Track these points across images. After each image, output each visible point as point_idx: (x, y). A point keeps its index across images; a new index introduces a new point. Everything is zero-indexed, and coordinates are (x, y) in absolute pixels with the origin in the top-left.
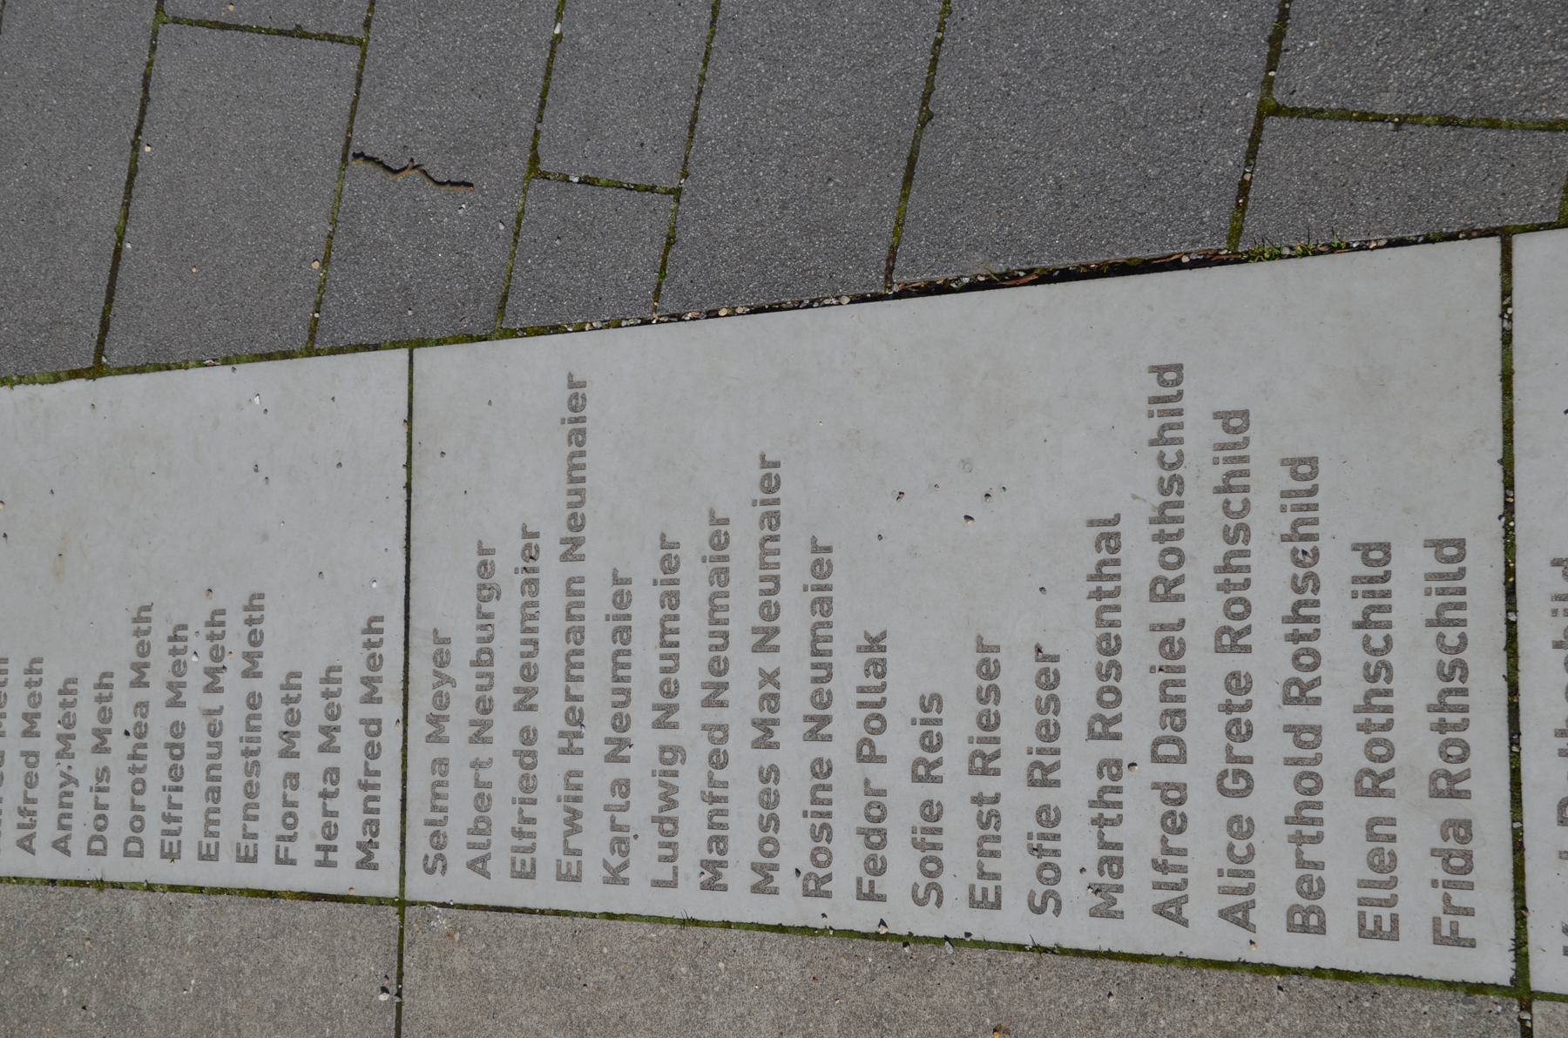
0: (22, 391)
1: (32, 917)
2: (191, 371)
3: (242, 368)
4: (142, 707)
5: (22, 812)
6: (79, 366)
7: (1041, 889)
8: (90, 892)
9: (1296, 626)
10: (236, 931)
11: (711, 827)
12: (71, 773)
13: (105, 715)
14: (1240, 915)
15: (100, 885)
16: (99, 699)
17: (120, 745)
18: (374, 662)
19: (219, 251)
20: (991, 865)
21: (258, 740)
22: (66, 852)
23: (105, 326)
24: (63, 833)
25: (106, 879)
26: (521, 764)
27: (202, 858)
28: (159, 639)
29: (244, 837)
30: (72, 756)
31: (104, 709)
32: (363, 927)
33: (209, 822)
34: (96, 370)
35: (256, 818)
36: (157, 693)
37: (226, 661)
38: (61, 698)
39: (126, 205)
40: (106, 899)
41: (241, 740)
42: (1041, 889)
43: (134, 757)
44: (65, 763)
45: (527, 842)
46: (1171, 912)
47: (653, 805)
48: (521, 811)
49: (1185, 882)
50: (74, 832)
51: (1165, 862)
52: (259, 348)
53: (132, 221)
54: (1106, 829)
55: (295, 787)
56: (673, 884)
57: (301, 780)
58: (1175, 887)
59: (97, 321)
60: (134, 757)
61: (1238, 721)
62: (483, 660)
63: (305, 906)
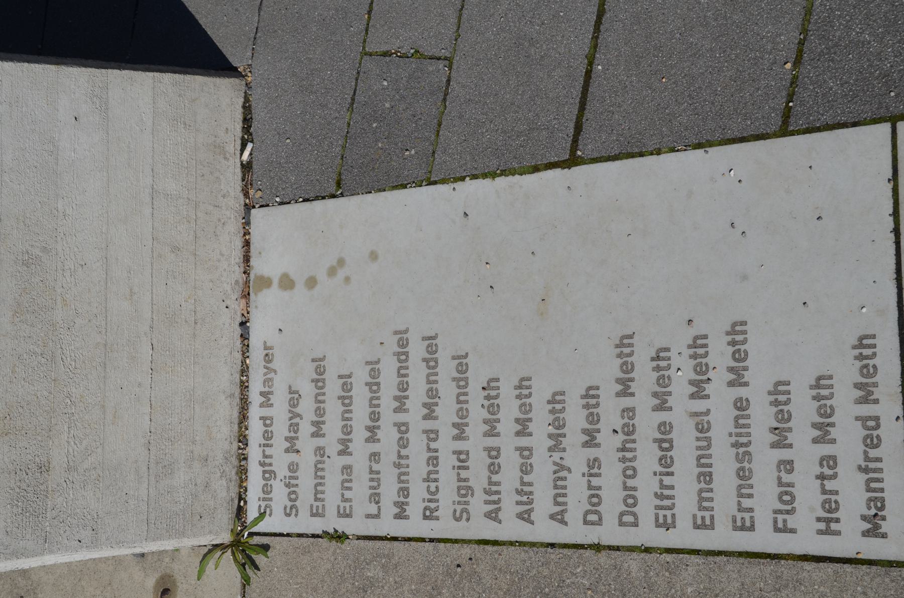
0: (501, 181)
1: (534, 572)
2: (662, 156)
3: (713, 151)
4: (629, 412)
5: (519, 492)
6: (556, 159)
7: (289, 504)
8: (588, 553)
9: (860, 351)
10: (737, 585)
11: (868, 491)
12: (563, 463)
13: (593, 419)
14: (559, 517)
15: (597, 548)
16: (587, 406)
17: (609, 442)
18: (869, 371)
19: (688, 64)
20: (747, 503)
21: (749, 435)
22: (563, 522)
23: (578, 128)
24: (558, 509)
25: (603, 543)
26: (661, 448)
27: (697, 527)
28: (642, 358)
29: (739, 510)
30: (564, 450)
31: (592, 414)
32: (875, 585)
33: (701, 499)
34: (572, 161)
35: (750, 496)
36: (643, 400)
37: (711, 374)
38: (550, 407)
39: (595, 38)
40: (603, 558)
41: (730, 435)
42: (289, 504)
43: (624, 449)
44: (556, 456)
45: (495, 498)
46: (525, 517)
47: (424, 470)
48: (459, 474)
49: (674, 504)
50: (570, 507)
51: (522, 490)
52: (729, 135)
53: (602, 48)
54: (825, 482)
55: (790, 471)
56: (377, 516)
57: (796, 465)
58: (494, 502)
59: (572, 125)
60: (624, 449)
61: (782, 411)
62: (374, 386)
63: (808, 566)
